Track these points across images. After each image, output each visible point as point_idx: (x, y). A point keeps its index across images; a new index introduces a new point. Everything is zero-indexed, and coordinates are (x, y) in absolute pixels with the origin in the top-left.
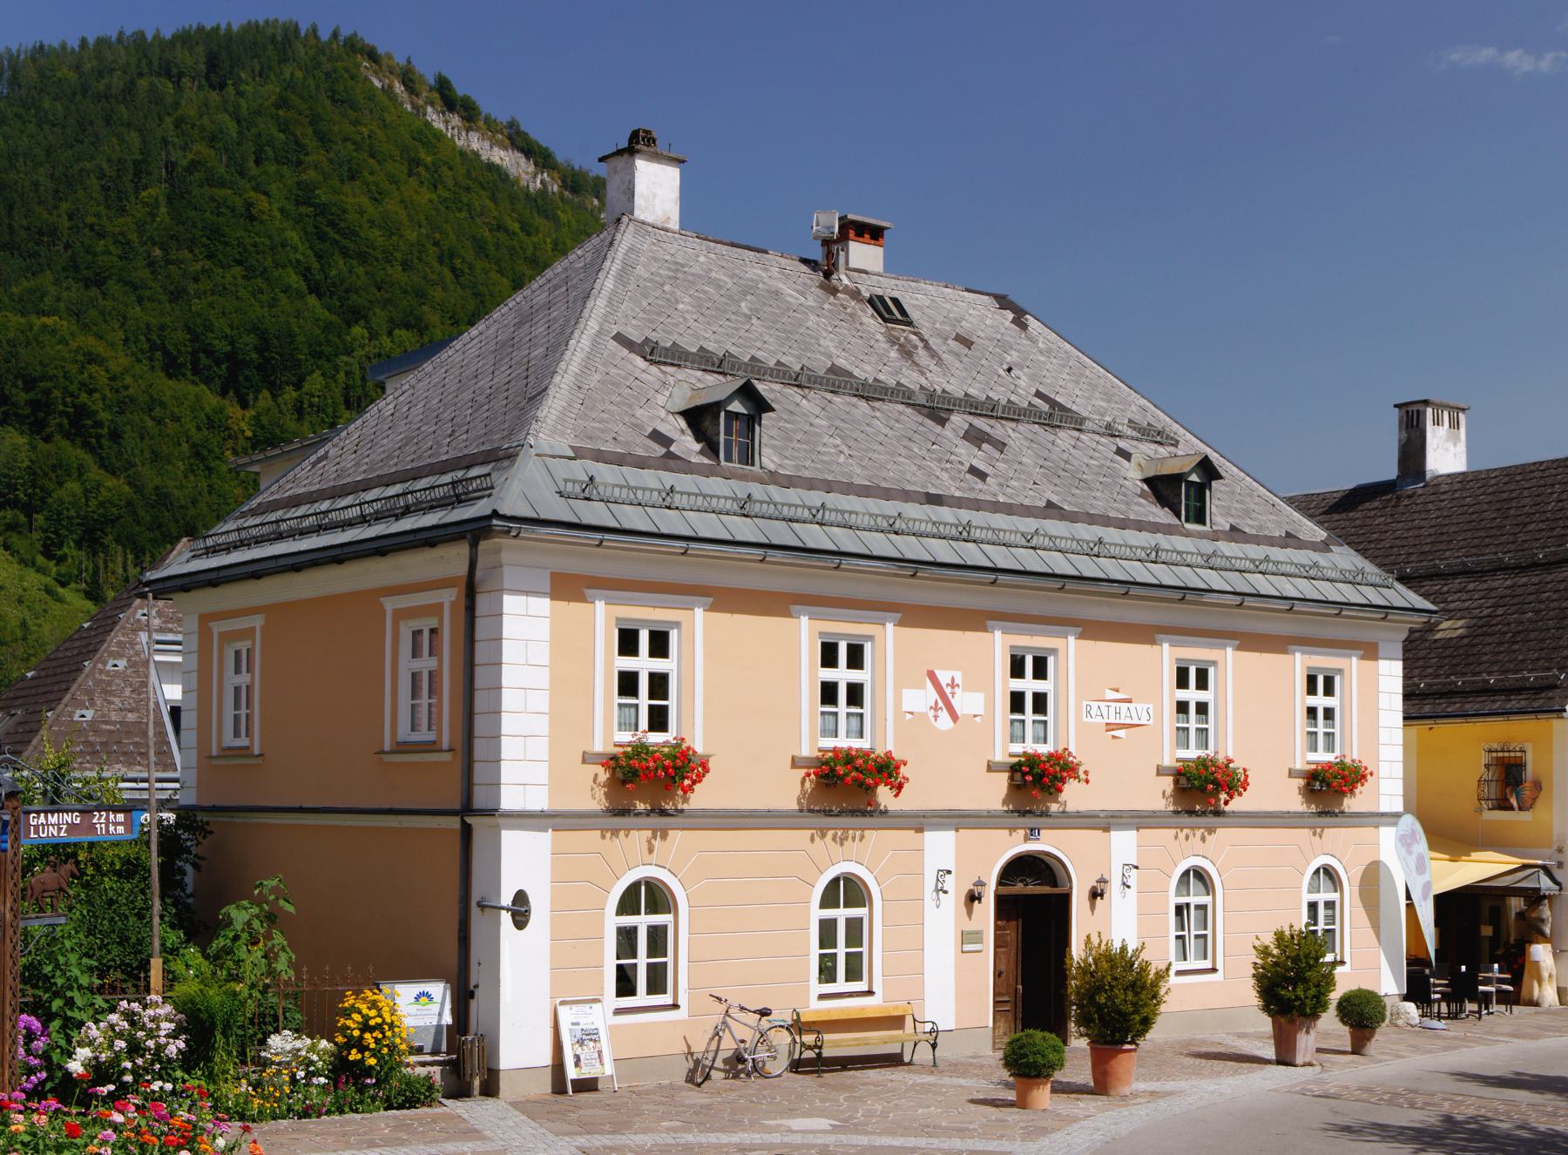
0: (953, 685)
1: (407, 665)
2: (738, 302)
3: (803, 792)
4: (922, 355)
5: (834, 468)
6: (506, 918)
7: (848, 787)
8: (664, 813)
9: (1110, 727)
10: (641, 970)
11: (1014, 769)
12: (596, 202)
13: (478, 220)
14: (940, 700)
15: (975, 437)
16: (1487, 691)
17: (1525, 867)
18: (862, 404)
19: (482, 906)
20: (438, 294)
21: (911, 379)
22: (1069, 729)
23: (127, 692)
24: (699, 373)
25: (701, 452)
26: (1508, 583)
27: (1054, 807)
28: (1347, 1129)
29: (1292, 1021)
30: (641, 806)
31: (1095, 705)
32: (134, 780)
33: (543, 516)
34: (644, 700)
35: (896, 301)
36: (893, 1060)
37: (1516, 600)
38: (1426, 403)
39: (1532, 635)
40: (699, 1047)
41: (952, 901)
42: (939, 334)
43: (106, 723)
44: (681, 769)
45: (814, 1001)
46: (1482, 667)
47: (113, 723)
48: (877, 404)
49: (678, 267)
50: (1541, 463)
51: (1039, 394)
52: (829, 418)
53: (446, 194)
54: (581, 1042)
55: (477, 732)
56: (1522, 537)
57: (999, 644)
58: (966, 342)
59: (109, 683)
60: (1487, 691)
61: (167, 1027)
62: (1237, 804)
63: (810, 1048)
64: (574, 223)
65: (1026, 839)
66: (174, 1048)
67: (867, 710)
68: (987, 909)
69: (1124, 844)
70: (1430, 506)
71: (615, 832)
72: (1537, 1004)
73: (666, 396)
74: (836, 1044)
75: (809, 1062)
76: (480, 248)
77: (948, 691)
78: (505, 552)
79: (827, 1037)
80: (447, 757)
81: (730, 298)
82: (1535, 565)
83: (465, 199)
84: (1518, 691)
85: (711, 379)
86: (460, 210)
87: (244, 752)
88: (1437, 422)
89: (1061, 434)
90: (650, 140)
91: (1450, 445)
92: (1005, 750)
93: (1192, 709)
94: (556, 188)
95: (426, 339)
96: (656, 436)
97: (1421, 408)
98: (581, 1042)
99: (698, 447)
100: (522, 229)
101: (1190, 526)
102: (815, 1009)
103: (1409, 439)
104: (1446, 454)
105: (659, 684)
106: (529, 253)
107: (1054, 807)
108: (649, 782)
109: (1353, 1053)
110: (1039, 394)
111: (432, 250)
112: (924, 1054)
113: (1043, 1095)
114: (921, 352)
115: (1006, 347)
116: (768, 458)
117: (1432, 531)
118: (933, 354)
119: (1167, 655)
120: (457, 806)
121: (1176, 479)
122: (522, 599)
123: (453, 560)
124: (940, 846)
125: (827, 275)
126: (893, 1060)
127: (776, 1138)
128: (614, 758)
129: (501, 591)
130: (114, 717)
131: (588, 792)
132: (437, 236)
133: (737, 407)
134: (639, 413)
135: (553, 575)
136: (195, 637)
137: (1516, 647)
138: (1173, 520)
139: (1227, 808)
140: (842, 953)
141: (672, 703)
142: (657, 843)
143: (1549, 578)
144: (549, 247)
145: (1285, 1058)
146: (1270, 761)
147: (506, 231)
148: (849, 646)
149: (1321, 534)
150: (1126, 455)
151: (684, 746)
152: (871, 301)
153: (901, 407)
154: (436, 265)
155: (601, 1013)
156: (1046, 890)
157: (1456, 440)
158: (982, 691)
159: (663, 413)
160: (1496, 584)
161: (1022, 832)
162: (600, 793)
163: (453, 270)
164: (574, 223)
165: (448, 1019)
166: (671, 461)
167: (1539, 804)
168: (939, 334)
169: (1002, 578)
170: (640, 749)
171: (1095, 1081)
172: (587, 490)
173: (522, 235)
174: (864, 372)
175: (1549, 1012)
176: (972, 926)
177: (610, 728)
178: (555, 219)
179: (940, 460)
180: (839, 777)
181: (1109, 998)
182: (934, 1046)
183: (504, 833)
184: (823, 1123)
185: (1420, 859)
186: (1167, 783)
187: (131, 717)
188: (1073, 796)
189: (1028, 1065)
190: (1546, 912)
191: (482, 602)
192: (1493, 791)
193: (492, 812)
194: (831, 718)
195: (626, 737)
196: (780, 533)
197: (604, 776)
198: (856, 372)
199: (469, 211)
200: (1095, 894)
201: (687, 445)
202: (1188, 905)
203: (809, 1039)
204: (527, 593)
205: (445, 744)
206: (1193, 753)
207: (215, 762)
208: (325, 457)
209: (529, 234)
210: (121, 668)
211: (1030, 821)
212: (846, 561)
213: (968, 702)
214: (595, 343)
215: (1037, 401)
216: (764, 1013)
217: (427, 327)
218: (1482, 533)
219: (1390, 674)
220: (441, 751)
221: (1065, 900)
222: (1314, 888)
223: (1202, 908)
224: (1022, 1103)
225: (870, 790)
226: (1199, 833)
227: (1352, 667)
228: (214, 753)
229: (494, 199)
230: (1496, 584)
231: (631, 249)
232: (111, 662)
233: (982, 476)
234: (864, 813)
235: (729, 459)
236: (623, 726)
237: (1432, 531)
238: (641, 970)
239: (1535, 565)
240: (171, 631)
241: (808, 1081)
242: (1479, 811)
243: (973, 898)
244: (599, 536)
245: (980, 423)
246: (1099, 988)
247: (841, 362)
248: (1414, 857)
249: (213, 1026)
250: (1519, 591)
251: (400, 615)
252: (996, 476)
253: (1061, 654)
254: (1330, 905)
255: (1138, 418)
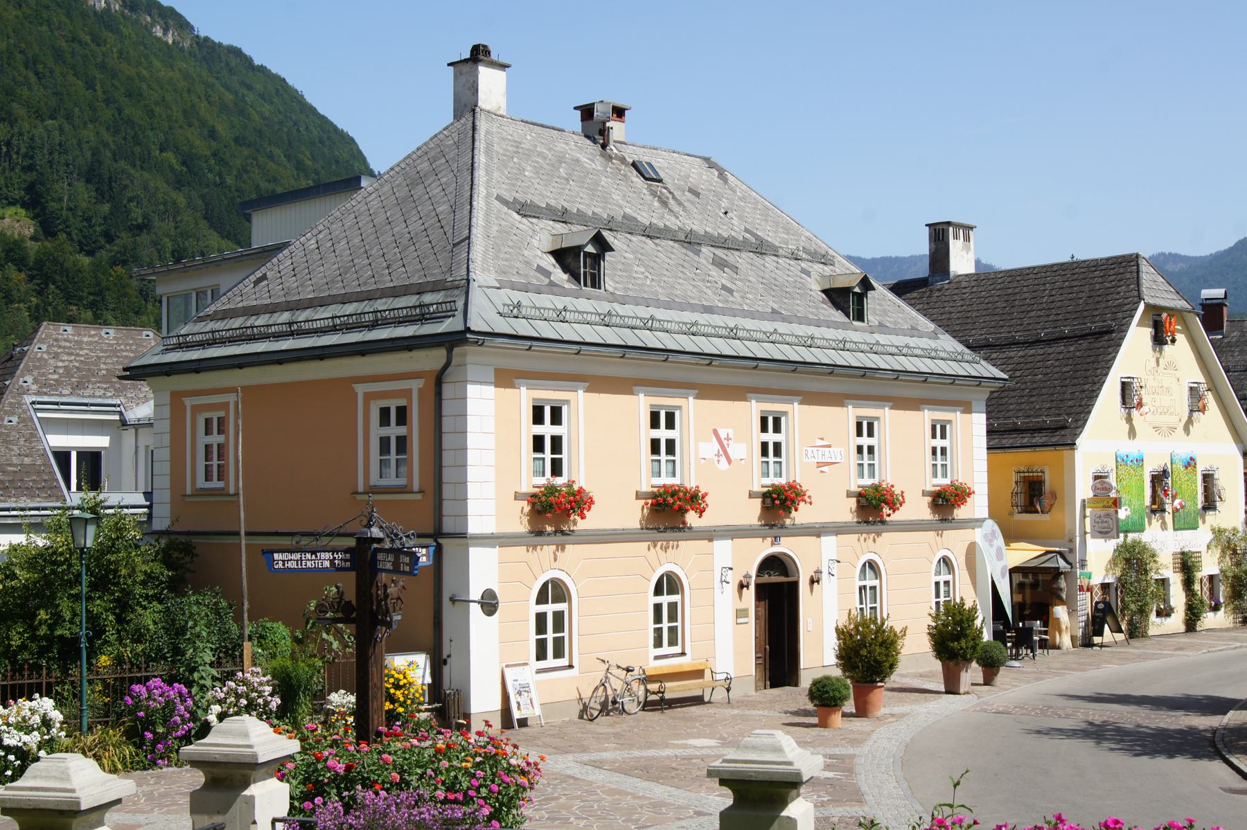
0: (728, 439)
1: (377, 432)
2: (558, 169)
3: (643, 516)
4: (676, 208)
5: (646, 289)
6: (475, 609)
7: (669, 511)
8: (563, 533)
9: (820, 465)
10: (551, 640)
11: (765, 496)
12: (149, 19)
13: (56, 33)
14: (720, 448)
15: (720, 264)
16: (1016, 430)
17: (1047, 552)
18: (648, 241)
19: (453, 600)
20: (25, 92)
21: (672, 222)
22: (797, 469)
23: (22, 441)
24: (551, 223)
25: (568, 281)
26: (1021, 353)
27: (788, 522)
28: (1039, 732)
29: (957, 664)
30: (549, 529)
31: (810, 449)
32: (22, 509)
33: (496, 331)
34: (548, 455)
35: (649, 164)
36: (698, 700)
37: (1028, 366)
38: (949, 223)
39: (1044, 391)
40: (586, 695)
41: (732, 588)
42: (679, 188)
43: (10, 465)
44: (578, 502)
45: (650, 660)
46: (1010, 414)
47: (16, 465)
48: (658, 241)
49: (517, 144)
50: (1034, 268)
51: (747, 230)
52: (633, 253)
53: (28, 12)
54: (520, 693)
55: (445, 479)
56: (1026, 321)
57: (754, 408)
58: (697, 194)
59: (8, 435)
60: (1016, 430)
61: (268, 689)
62: (897, 516)
63: (654, 693)
64: (133, 35)
65: (773, 544)
66: (276, 702)
67: (677, 458)
68: (750, 594)
69: (829, 544)
70: (956, 297)
71: (535, 547)
72: (1059, 648)
73: (542, 237)
74: (672, 690)
75: (654, 703)
76: (59, 55)
77: (725, 443)
78: (469, 355)
79: (668, 685)
80: (419, 497)
81: (552, 165)
82: (1038, 341)
83: (45, 16)
84: (1039, 430)
85: (559, 226)
86: (41, 25)
87: (222, 492)
88: (956, 237)
89: (767, 259)
90: (487, 52)
91: (964, 253)
92: (761, 483)
93: (865, 450)
94: (117, 7)
95: (16, 130)
96: (540, 269)
97: (945, 227)
98: (520, 693)
99: (566, 277)
100: (93, 41)
101: (856, 323)
102: (654, 667)
103: (936, 249)
104: (961, 262)
105: (557, 442)
106: (99, 60)
107: (788, 522)
108: (554, 512)
109: (985, 684)
110: (747, 230)
111: (19, 57)
112: (720, 694)
113: (836, 718)
114: (672, 201)
115: (719, 197)
116: (609, 283)
117: (959, 315)
118: (680, 203)
119: (851, 413)
120: (430, 530)
121: (845, 291)
122: (478, 387)
123: (431, 359)
124: (723, 550)
125: (604, 146)
126: (698, 700)
127: (679, 752)
128: (534, 496)
129: (466, 382)
130: (15, 460)
131: (518, 523)
132: (23, 45)
133: (590, 249)
134: (526, 253)
135: (496, 370)
136: (168, 408)
137: (1033, 399)
138: (846, 320)
139: (888, 519)
140: (667, 626)
141: (564, 456)
142: (559, 554)
143: (1050, 351)
144: (116, 55)
145: (952, 687)
146: (912, 484)
147: (80, 42)
148: (667, 413)
149: (932, 326)
150: (806, 272)
151: (576, 487)
152: (634, 165)
153: (671, 243)
154: (22, 69)
155: (526, 674)
156: (782, 579)
157: (968, 249)
158: (746, 444)
159: (539, 253)
160: (1012, 354)
161: (769, 539)
162: (525, 520)
163: (37, 74)
164: (133, 35)
165: (428, 680)
166: (553, 288)
167: (1053, 509)
168: (679, 188)
169: (762, 364)
170: (551, 490)
171: (857, 708)
172: (515, 311)
173: (93, 46)
174: (644, 218)
175: (1068, 653)
176: (742, 606)
177: (531, 478)
178: (117, 31)
179: (703, 281)
180: (668, 505)
181: (869, 652)
182: (728, 690)
183: (471, 549)
184: (712, 742)
185: (999, 549)
186: (853, 502)
187: (27, 460)
188: (802, 515)
189: (827, 699)
190: (1063, 584)
191: (447, 390)
192: (1021, 500)
193: (463, 535)
194: (656, 464)
195: (542, 481)
196: (631, 339)
197: (527, 508)
198: (639, 218)
199: (49, 25)
200: (812, 582)
201: (559, 276)
202: (865, 587)
203: (654, 687)
204: (481, 383)
205: (416, 487)
206: (867, 481)
207: (187, 499)
208: (264, 277)
209: (98, 45)
210: (14, 423)
211: (775, 531)
212: (672, 357)
213: (737, 450)
214: (488, 204)
215: (747, 236)
216: (628, 670)
217: (16, 120)
218: (997, 318)
219: (978, 422)
220: (412, 492)
221: (794, 586)
222: (938, 573)
223: (873, 588)
224: (823, 724)
225: (682, 511)
226: (872, 536)
227: (957, 418)
228: (189, 492)
229: (69, 15)
230: (1012, 354)
231: (487, 132)
232: (7, 419)
233: (730, 291)
234: (680, 530)
235: (585, 285)
236: (536, 473)
237: (959, 315)
238: (551, 640)
239: (1038, 341)
240: (46, 394)
241: (655, 716)
242: (1011, 514)
243: (742, 586)
244: (529, 343)
245: (719, 252)
246: (862, 644)
247: (628, 211)
248: (995, 549)
249: (299, 686)
250: (1030, 359)
251: (369, 397)
252: (738, 291)
253: (790, 415)
254: (947, 583)
255: (807, 246)
